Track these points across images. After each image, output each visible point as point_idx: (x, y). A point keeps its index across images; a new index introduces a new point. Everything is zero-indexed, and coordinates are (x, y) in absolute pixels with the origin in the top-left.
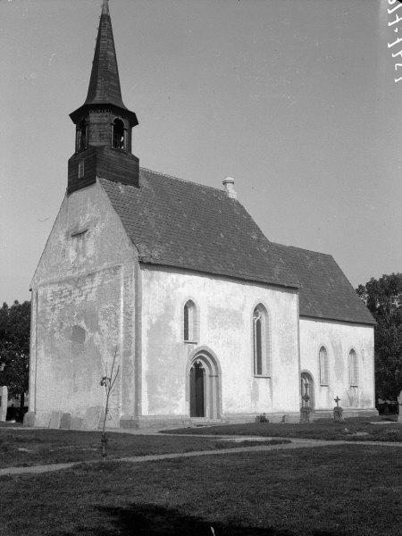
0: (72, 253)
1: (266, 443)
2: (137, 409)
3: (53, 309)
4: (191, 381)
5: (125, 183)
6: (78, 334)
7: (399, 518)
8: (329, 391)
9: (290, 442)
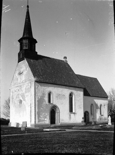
0: (19, 80)
1: (59, 131)
3: (15, 95)
6: (21, 102)
8: (94, 117)
9: (65, 130)
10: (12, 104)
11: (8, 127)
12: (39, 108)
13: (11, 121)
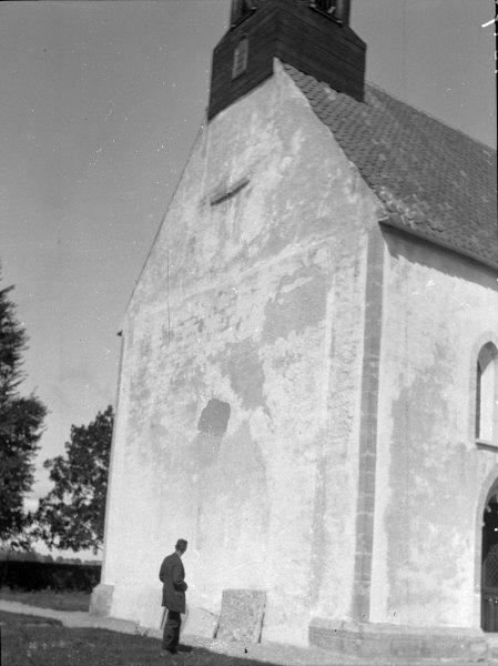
0: (210, 240)
2: (361, 605)
3: (162, 367)
4: (480, 571)
5: (337, 88)
6: (217, 414)
7: (3, 642)
10: (130, 441)
11: (72, 620)
12: (400, 472)
13: (107, 578)
